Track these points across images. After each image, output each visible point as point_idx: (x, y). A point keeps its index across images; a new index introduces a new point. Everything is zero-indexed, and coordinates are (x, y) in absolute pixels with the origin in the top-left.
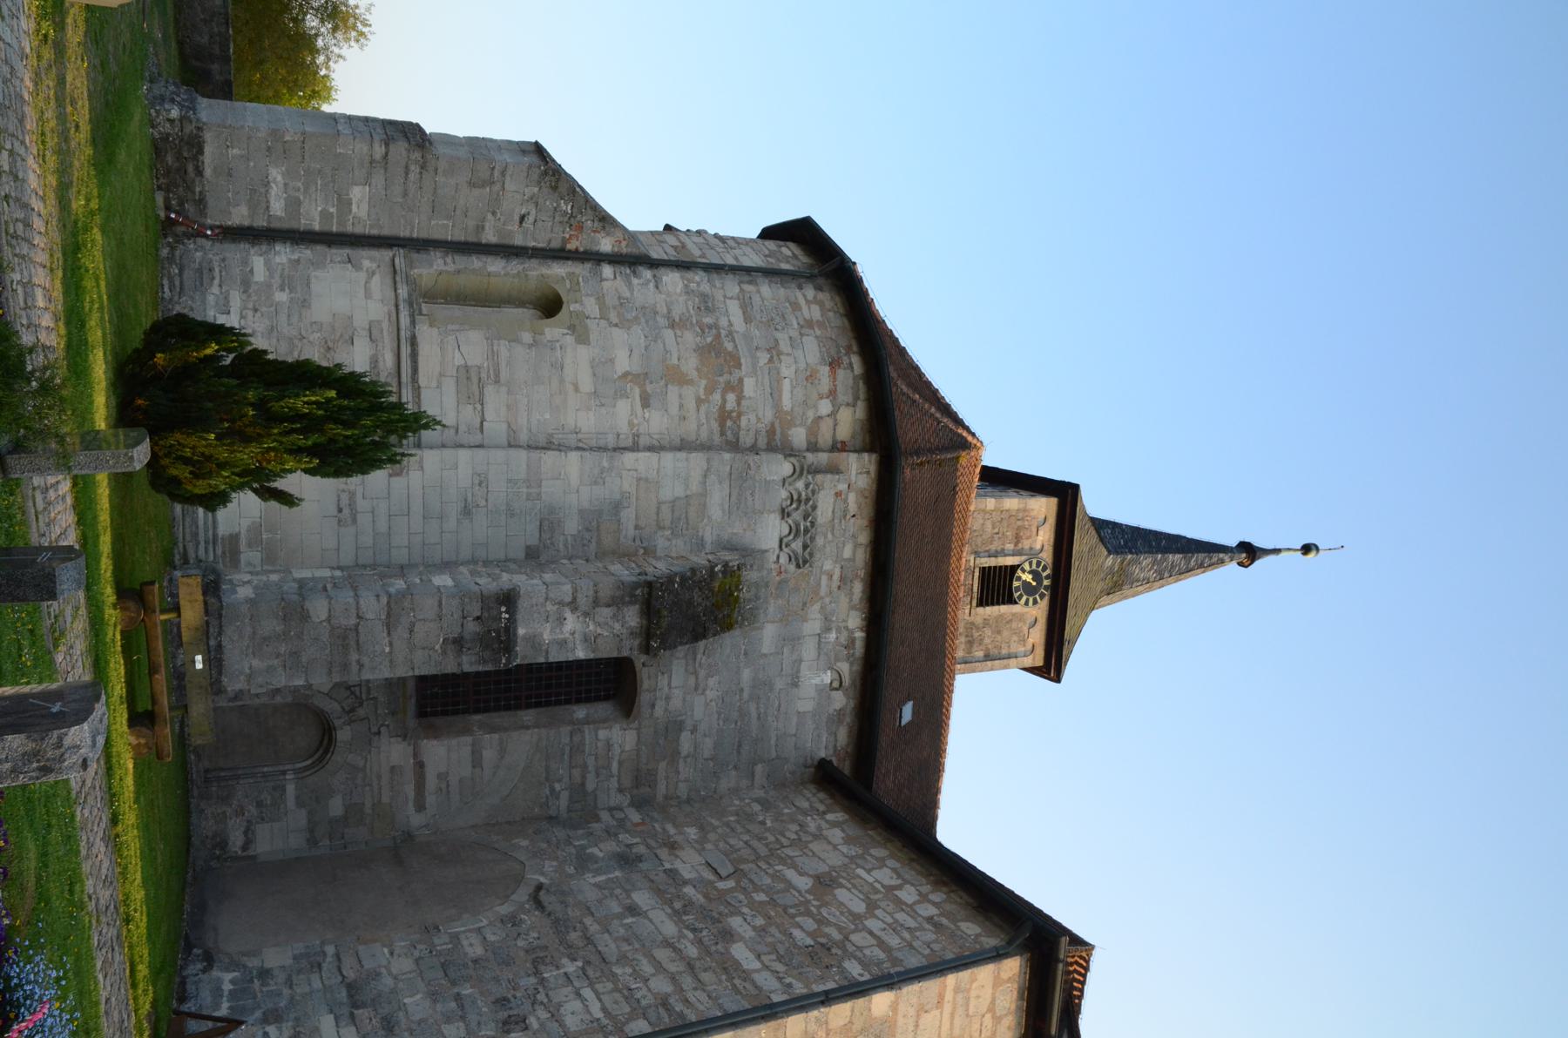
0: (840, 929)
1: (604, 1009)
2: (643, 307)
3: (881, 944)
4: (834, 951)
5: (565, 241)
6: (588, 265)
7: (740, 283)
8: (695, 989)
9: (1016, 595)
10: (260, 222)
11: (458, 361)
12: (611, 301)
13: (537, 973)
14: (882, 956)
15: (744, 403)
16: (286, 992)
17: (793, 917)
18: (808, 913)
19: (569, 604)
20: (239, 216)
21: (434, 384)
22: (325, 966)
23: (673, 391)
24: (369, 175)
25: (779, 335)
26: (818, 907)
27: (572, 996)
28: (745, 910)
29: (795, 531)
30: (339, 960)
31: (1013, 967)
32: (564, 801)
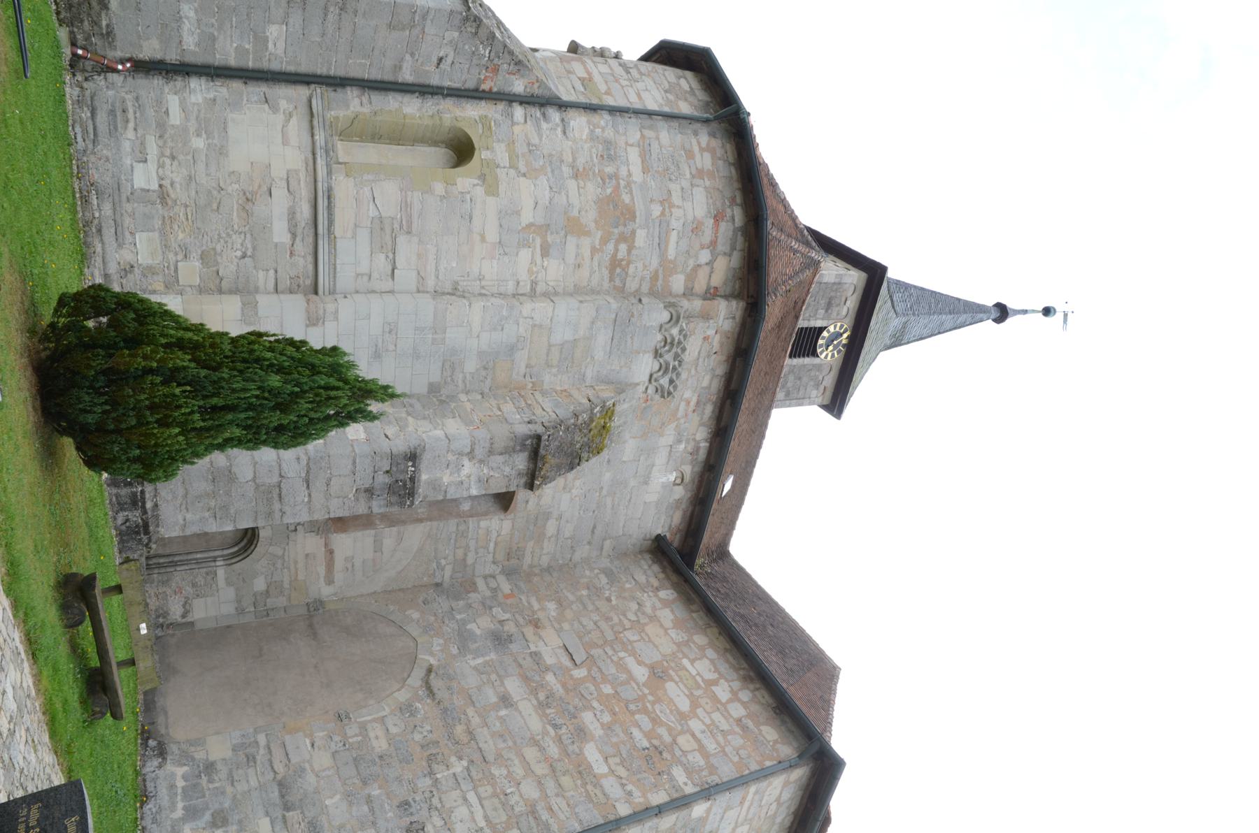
0: (670, 730)
1: (486, 817)
2: (550, 155)
3: (702, 749)
4: (665, 755)
5: (480, 82)
6: (501, 106)
7: (642, 128)
8: (557, 795)
9: (819, 351)
10: (172, 57)
11: (372, 212)
12: (521, 148)
13: (431, 773)
14: (702, 763)
15: (634, 252)
16: (229, 789)
17: (633, 713)
18: (645, 711)
19: (468, 454)
20: (150, 50)
21: (349, 234)
22: (258, 758)
23: (572, 241)
24: (287, 15)
25: (672, 186)
26: (653, 703)
27: (460, 801)
28: (595, 704)
29: (664, 368)
30: (270, 752)
31: (800, 774)
32: (448, 572)
